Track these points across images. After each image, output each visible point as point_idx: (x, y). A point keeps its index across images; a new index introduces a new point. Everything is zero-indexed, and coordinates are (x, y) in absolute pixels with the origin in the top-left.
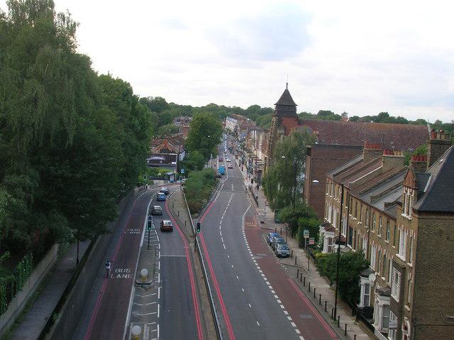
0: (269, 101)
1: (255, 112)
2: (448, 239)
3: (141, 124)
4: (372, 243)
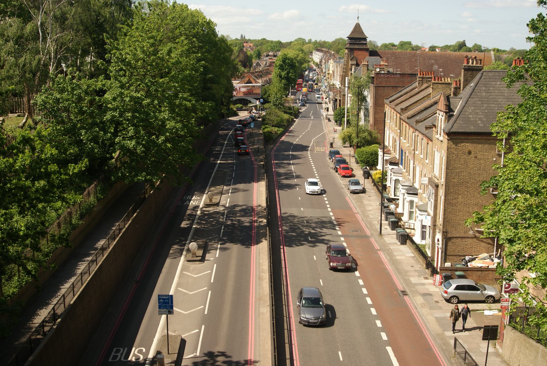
0: (345, 33)
1: (338, 42)
2: (476, 157)
3: (192, 69)
4: (416, 163)
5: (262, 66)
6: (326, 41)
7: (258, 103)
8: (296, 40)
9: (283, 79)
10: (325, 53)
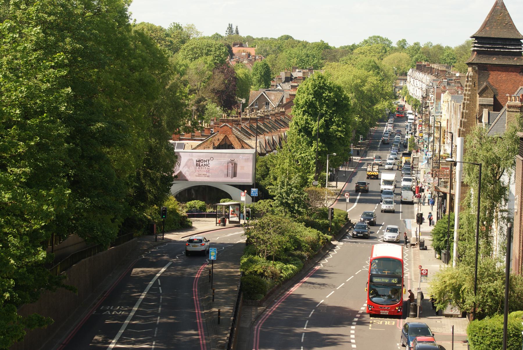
5: (273, 104)
6: (444, 45)
7: (243, 199)
8: (366, 42)
9: (315, 138)
10: (437, 76)
